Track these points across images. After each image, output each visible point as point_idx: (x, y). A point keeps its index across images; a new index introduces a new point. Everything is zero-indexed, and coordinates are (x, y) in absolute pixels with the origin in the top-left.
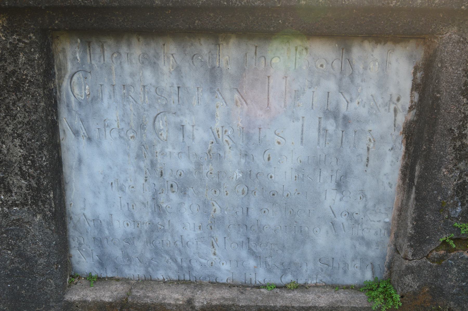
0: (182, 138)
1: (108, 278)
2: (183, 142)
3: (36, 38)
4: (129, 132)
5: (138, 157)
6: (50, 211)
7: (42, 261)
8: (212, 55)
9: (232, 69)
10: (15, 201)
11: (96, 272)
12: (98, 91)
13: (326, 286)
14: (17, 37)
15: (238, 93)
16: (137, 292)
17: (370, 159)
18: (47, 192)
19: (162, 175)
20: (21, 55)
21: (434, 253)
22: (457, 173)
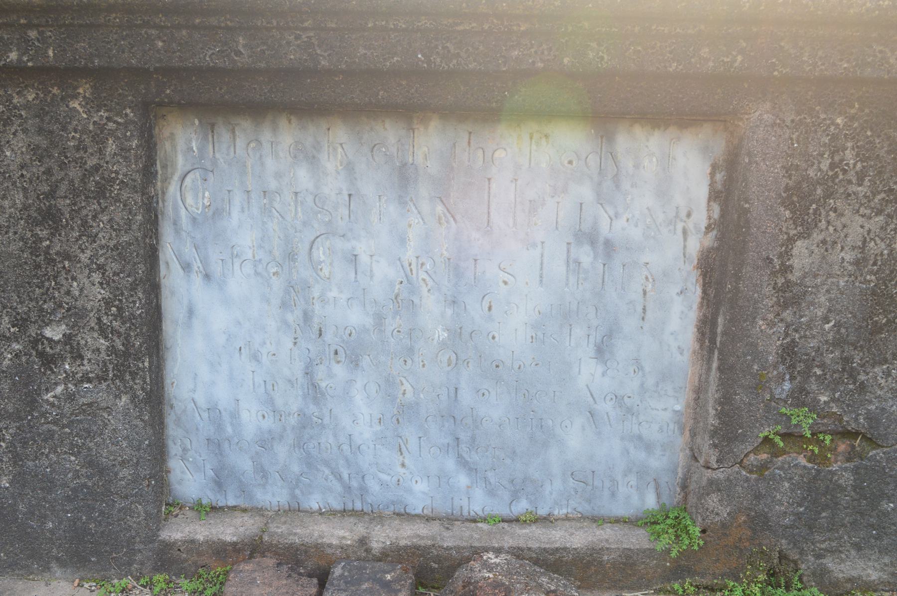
0: (353, 275)
1: (229, 508)
3: (135, 116)
6: (143, 389)
7: (125, 472)
8: (403, 145)
11: (210, 497)
12: (223, 200)
13: (583, 518)
14: (106, 114)
16: (277, 527)
17: (647, 308)
18: (140, 359)
19: (320, 335)
20: (111, 142)
21: (752, 457)
22: (781, 327)
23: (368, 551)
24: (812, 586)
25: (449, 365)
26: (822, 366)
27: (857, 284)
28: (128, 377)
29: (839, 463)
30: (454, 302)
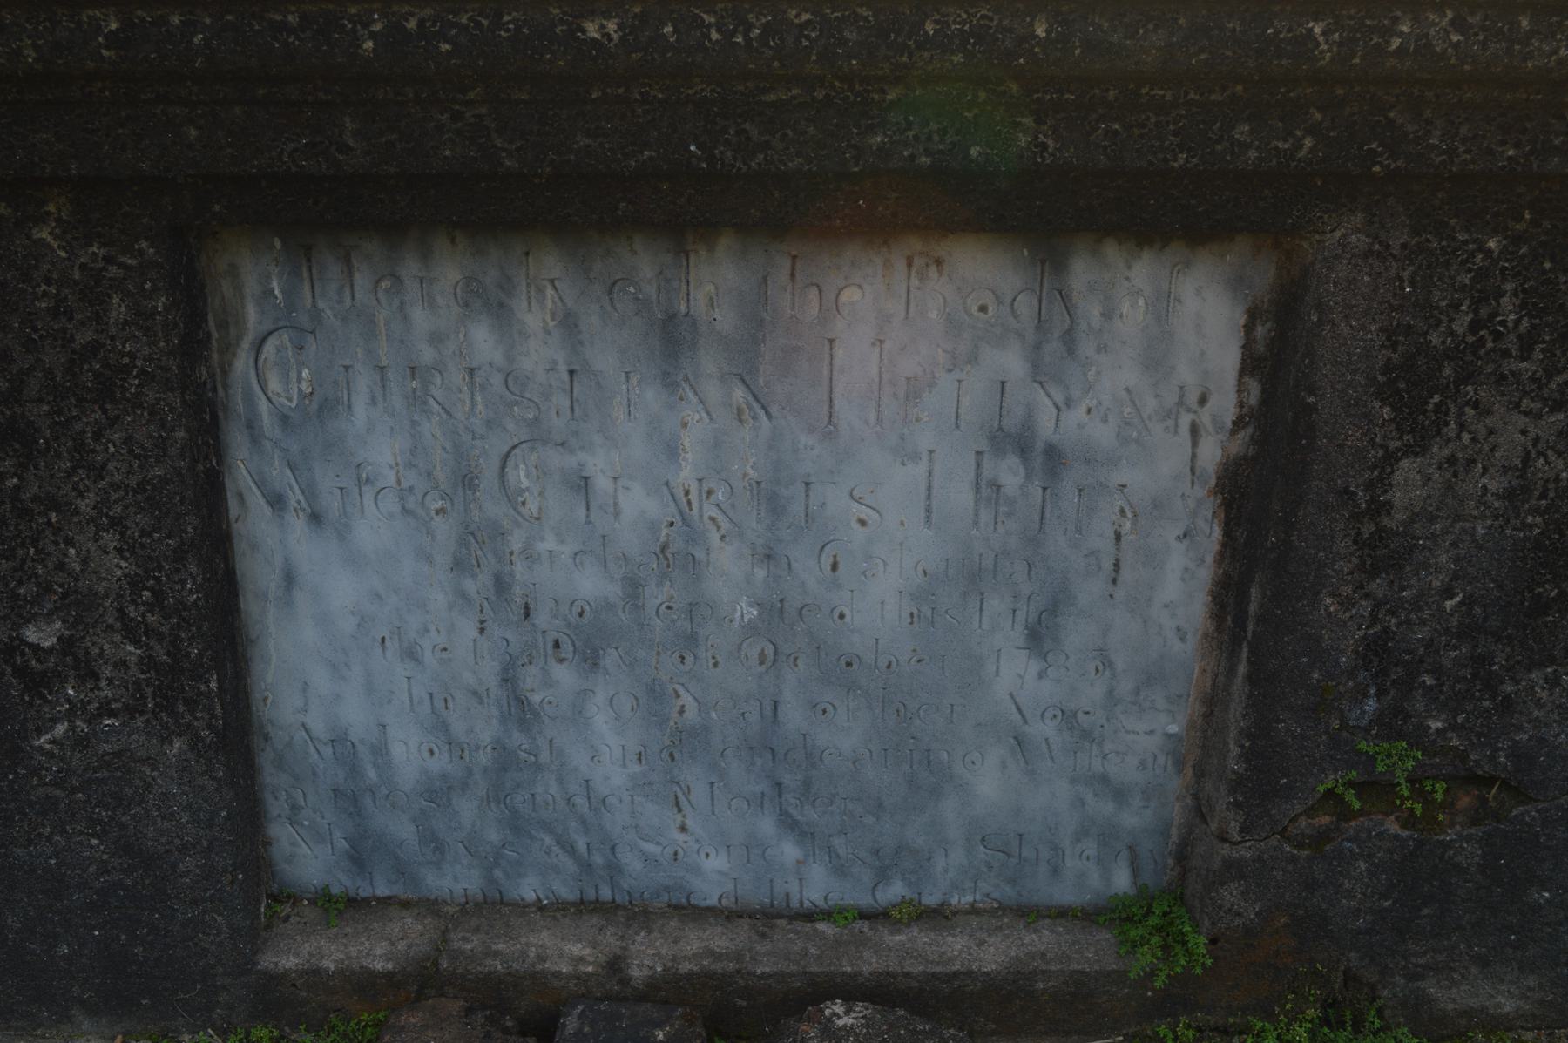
0: (582, 512)
1: (379, 900)
2: (588, 522)
4: (428, 497)
5: (459, 565)
7: (189, 863)
9: (726, 319)
10: (108, 703)
11: (343, 882)
12: (336, 383)
13: (1002, 909)
14: (103, 252)
15: (743, 387)
16: (465, 939)
17: (1122, 564)
19: (527, 615)
20: (115, 300)
21: (1303, 822)
22: (1366, 607)
23: (625, 981)
24: (1398, 1025)
25: (761, 663)
26: (1437, 671)
27: (1508, 532)
28: (181, 708)
29: (1458, 827)
30: (769, 557)
